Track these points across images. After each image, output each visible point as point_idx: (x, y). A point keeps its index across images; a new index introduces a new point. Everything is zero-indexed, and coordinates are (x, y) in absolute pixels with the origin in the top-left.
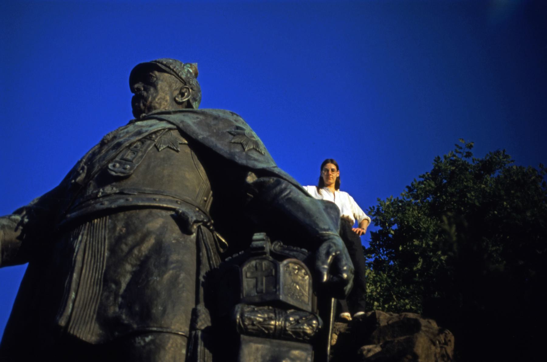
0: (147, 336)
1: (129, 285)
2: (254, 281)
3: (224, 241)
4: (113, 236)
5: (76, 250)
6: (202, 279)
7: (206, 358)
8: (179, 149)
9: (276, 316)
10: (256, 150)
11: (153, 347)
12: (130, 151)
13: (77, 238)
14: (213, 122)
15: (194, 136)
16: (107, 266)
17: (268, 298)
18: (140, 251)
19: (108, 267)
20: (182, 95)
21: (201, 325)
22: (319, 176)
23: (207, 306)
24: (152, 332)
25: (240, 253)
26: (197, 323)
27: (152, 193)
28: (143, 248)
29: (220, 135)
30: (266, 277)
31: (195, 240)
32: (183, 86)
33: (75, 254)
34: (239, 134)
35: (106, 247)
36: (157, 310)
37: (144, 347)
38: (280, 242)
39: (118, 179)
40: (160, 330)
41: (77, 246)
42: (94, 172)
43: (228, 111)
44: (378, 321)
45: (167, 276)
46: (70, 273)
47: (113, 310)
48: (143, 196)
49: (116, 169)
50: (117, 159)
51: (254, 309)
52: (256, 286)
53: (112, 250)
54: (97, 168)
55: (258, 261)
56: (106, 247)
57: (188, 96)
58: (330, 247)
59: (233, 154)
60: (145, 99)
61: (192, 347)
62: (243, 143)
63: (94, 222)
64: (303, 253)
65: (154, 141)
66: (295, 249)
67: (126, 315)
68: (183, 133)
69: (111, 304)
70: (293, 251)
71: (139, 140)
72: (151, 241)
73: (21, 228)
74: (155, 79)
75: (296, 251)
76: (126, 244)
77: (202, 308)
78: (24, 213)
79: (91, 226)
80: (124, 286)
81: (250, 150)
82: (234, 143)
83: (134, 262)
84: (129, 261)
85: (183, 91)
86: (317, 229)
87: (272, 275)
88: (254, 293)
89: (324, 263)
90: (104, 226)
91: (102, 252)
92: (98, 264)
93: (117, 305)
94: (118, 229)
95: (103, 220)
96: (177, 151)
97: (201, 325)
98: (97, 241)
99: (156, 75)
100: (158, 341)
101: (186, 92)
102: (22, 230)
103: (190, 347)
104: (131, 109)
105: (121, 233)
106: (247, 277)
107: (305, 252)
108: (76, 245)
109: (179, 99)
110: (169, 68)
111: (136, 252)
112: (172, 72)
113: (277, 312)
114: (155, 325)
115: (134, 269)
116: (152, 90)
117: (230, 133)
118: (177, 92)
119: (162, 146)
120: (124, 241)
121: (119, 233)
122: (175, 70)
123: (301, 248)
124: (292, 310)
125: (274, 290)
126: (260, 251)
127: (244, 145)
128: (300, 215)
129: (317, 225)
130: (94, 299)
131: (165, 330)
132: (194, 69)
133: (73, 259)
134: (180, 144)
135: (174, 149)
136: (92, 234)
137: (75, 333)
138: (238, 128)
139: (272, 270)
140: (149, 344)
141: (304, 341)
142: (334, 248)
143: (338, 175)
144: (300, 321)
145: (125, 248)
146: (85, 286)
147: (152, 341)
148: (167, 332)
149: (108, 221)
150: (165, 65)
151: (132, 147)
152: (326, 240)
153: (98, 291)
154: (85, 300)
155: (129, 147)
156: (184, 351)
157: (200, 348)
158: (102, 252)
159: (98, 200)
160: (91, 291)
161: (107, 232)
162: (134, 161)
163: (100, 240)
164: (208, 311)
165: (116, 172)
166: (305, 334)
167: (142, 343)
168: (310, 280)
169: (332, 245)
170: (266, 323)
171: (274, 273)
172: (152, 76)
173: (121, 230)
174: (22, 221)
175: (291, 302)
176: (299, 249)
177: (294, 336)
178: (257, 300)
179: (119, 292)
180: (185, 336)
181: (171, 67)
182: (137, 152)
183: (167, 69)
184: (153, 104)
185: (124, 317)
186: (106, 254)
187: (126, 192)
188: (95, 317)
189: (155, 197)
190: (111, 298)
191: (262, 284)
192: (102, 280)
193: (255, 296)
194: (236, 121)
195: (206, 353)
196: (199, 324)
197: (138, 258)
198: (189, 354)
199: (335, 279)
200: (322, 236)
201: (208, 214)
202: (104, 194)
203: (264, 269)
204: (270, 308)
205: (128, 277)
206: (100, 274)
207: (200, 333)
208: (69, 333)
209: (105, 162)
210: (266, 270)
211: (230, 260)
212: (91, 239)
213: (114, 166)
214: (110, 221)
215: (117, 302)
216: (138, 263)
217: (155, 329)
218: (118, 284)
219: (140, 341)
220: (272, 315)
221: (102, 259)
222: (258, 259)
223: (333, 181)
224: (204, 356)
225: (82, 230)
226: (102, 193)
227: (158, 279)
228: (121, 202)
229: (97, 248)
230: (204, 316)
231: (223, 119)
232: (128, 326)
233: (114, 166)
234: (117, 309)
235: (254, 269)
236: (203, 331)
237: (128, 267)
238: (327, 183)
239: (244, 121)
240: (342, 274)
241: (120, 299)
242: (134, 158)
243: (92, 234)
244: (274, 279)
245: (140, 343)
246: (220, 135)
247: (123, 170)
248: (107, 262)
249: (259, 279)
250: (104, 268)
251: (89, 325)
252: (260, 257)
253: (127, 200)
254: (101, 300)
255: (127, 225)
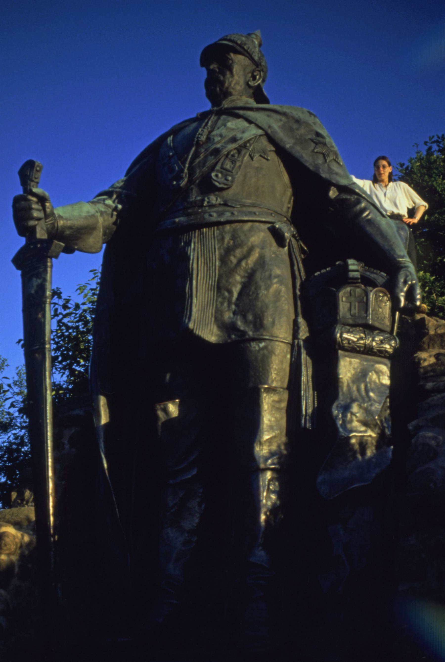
0: (261, 343)
1: (240, 294)
2: (348, 305)
3: (306, 248)
4: (222, 247)
5: (192, 257)
6: (298, 293)
7: (308, 364)
8: (269, 158)
9: (366, 337)
10: (335, 160)
11: (265, 352)
12: (228, 160)
13: (190, 245)
14: (295, 126)
15: (282, 144)
16: (219, 275)
17: (361, 322)
18: (247, 264)
19: (220, 276)
20: (254, 78)
21: (303, 336)
22: (373, 173)
23: (304, 317)
24: (264, 340)
25: (328, 269)
26: (299, 334)
27: (251, 205)
28: (249, 262)
29: (301, 141)
30: (358, 302)
31: (287, 252)
32: (255, 69)
33: (191, 262)
34: (320, 143)
35: (217, 257)
36: (268, 321)
37: (259, 351)
38: (362, 263)
39: (222, 189)
40: (271, 338)
41: (192, 254)
42: (195, 177)
43: (305, 110)
44: (427, 327)
45: (272, 290)
46: (189, 279)
47: (228, 316)
48: (244, 209)
49: (219, 180)
50: (218, 168)
51: (349, 329)
52: (350, 310)
53: (224, 260)
54: (198, 173)
55: (352, 288)
56: (217, 257)
57: (259, 79)
58: (407, 276)
59: (317, 166)
60: (222, 83)
61: (296, 354)
62: (325, 153)
63: (203, 231)
64: (382, 276)
65: (248, 149)
66: (375, 271)
67: (241, 322)
68: (271, 140)
69: (226, 309)
70: (373, 273)
71: (235, 149)
72: (255, 255)
73: (115, 213)
74: (231, 62)
75: (376, 274)
76: (235, 256)
77: (301, 320)
78: (115, 196)
79: (201, 234)
80: (235, 295)
81: (330, 161)
82: (317, 152)
83: (242, 273)
84: (238, 272)
85: (255, 74)
86: (395, 255)
87: (364, 302)
88: (348, 316)
89: (402, 291)
90: (213, 236)
91: (214, 261)
92: (211, 272)
93: (231, 311)
94: (226, 240)
95: (211, 230)
96: (267, 160)
97: (303, 336)
98: (208, 250)
99: (232, 58)
100: (270, 347)
101: (258, 75)
102: (117, 216)
103: (294, 353)
104: (204, 91)
105: (229, 245)
106: (342, 301)
107: (384, 275)
108: (190, 253)
109: (251, 83)
110: (243, 48)
111: (243, 264)
112: (246, 53)
113: (366, 333)
114: (268, 334)
115: (243, 280)
116: (228, 73)
117: (312, 140)
118: (250, 75)
119: (256, 156)
120: (232, 253)
121: (227, 245)
122: (249, 51)
123: (381, 271)
124: (377, 331)
125: (365, 315)
126: (355, 281)
127: (326, 156)
128: (379, 239)
129: (395, 251)
130: (210, 304)
131: (275, 339)
132: (259, 40)
133: (190, 266)
134: (270, 151)
135: (264, 158)
136: (202, 243)
137: (200, 333)
138: (318, 134)
139: (363, 298)
140: (262, 349)
141: (385, 357)
142: (410, 277)
143: (390, 171)
144: (383, 342)
145: (234, 260)
146: (201, 291)
147: (265, 347)
148: (277, 341)
149: (217, 232)
150: (240, 45)
151: (230, 156)
152: (402, 267)
153: (212, 296)
154: (203, 304)
155: (227, 155)
156: (289, 356)
157: (304, 355)
158: (214, 261)
159: (204, 209)
160: (206, 296)
161: (216, 242)
162: (233, 171)
163: (211, 250)
164: (306, 323)
165: (220, 183)
166: (386, 352)
167: (257, 348)
168: (390, 305)
169: (408, 273)
170: (358, 342)
171: (365, 300)
172: (228, 58)
173: (229, 242)
174: (116, 207)
175: (377, 324)
176: (379, 272)
177: (378, 353)
178: (351, 322)
179: (232, 300)
180: (288, 343)
181: (245, 47)
182: (235, 162)
183: (242, 50)
184: (229, 90)
185: (239, 323)
186: (217, 264)
187: (230, 204)
188: (213, 319)
189: (254, 210)
190: (226, 304)
191: (355, 308)
192: (216, 287)
193: (349, 318)
194: (315, 123)
195: (308, 360)
196: (301, 334)
197: (246, 271)
198: (293, 359)
199: (410, 305)
200: (399, 262)
201: (289, 218)
202: (210, 204)
203: (357, 296)
204: (361, 328)
205: (239, 287)
206: (213, 281)
207: (302, 343)
208: (195, 334)
209: (205, 169)
210: (359, 296)
211: (319, 275)
212: (202, 248)
213: (217, 176)
214: (218, 231)
215: (231, 308)
216: (246, 275)
217: (267, 337)
218: (230, 292)
219: (254, 346)
220: (362, 335)
221: (214, 267)
222: (352, 286)
223: (385, 177)
224: (307, 363)
225: (193, 237)
226: (208, 202)
227: (266, 292)
228: (227, 216)
229: (208, 257)
230: (303, 327)
231: (304, 122)
232: (244, 333)
233: (217, 176)
234: (232, 315)
235: (349, 294)
236: (304, 341)
237: (238, 278)
238: (379, 179)
239: (321, 124)
240: (416, 302)
241: (233, 307)
242: (233, 168)
243: (202, 243)
244: (365, 305)
245: (255, 347)
246: (301, 141)
247: (225, 181)
248: (219, 270)
249: (353, 304)
250: (217, 276)
251: (209, 327)
252: (354, 285)
253: (233, 214)
254: (216, 305)
255: (234, 237)
